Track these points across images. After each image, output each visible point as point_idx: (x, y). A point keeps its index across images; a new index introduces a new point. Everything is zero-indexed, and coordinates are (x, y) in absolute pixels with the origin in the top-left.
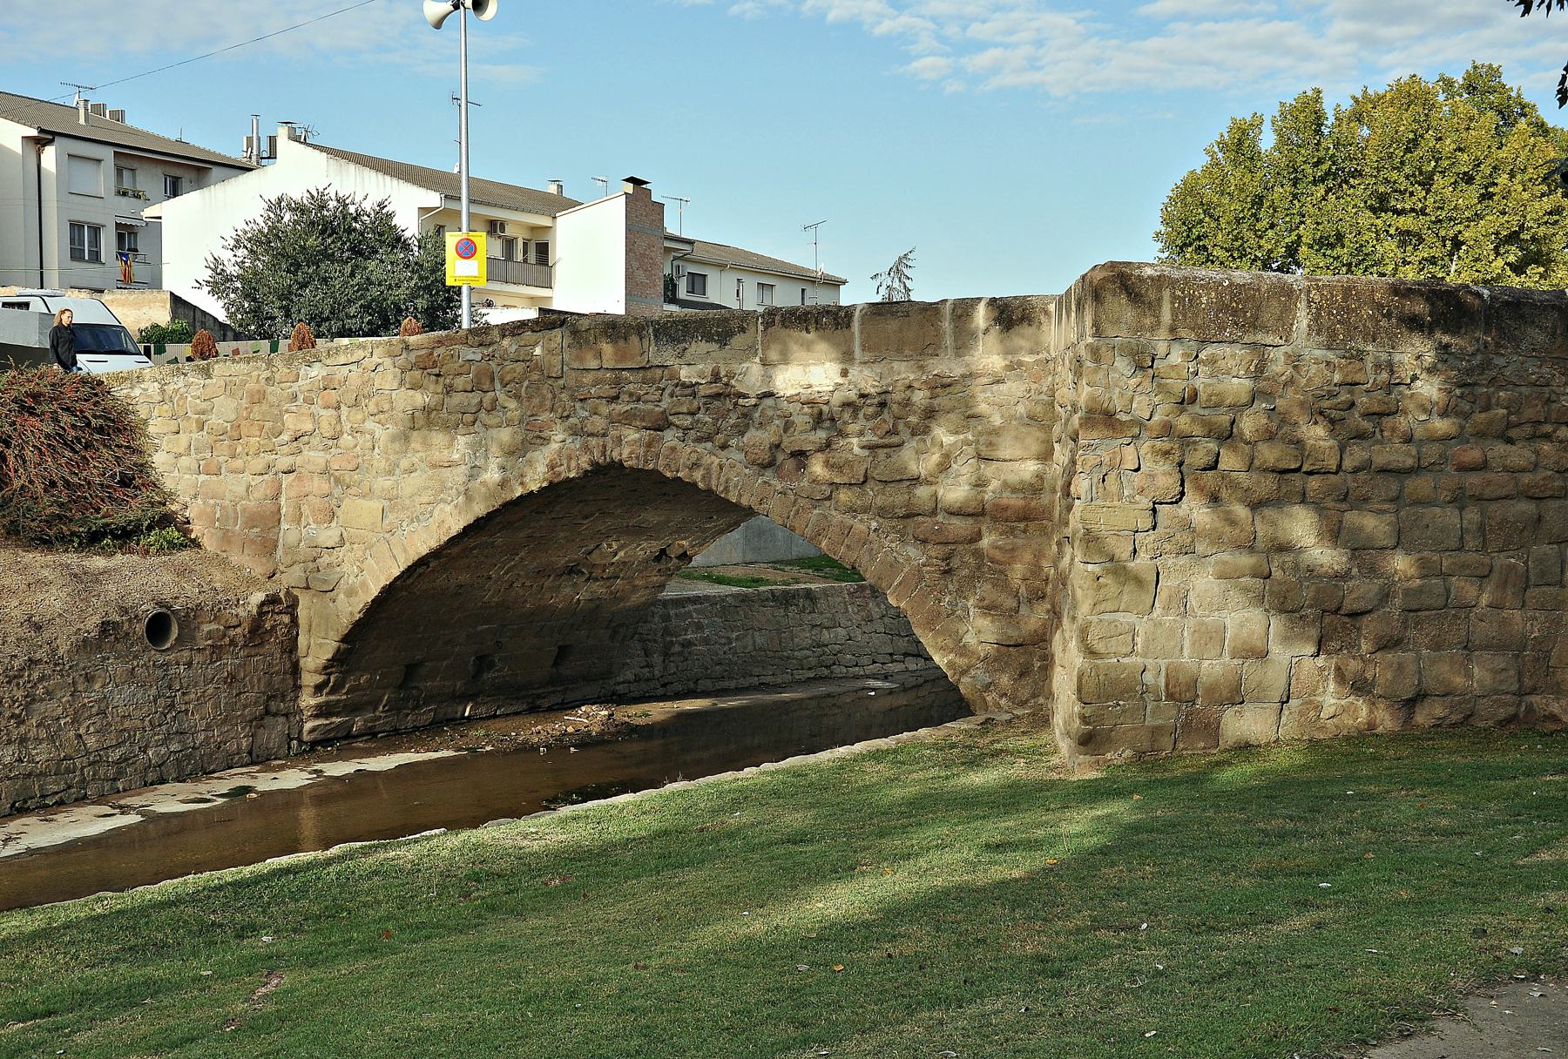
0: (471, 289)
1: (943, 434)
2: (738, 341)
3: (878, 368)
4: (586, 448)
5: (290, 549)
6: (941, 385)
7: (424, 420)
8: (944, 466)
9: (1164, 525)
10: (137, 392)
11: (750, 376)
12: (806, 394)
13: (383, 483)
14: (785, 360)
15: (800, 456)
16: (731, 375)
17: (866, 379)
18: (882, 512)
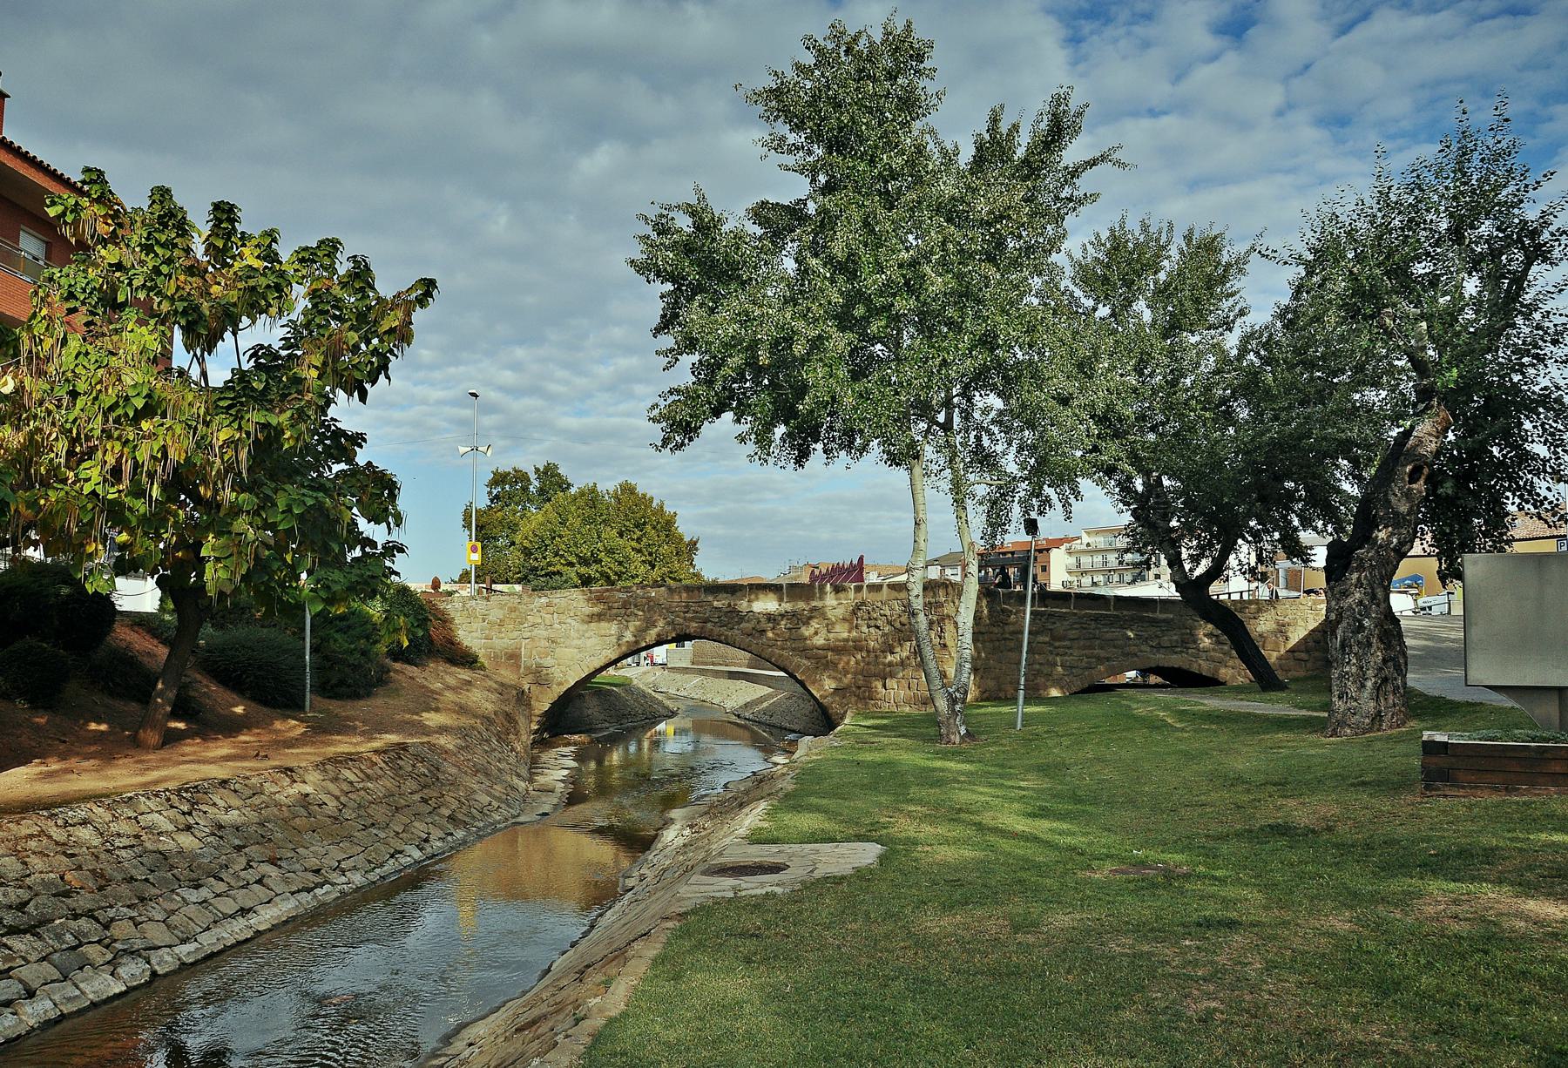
0: (470, 582)
1: (814, 624)
2: (738, 594)
3: (792, 604)
4: (674, 629)
5: (527, 668)
6: (815, 609)
7: (599, 617)
8: (816, 633)
9: (642, 961)
10: (449, 606)
11: (743, 605)
12: (765, 612)
13: (576, 642)
14: (757, 599)
15: (764, 631)
16: (735, 605)
17: (787, 606)
18: (793, 650)
